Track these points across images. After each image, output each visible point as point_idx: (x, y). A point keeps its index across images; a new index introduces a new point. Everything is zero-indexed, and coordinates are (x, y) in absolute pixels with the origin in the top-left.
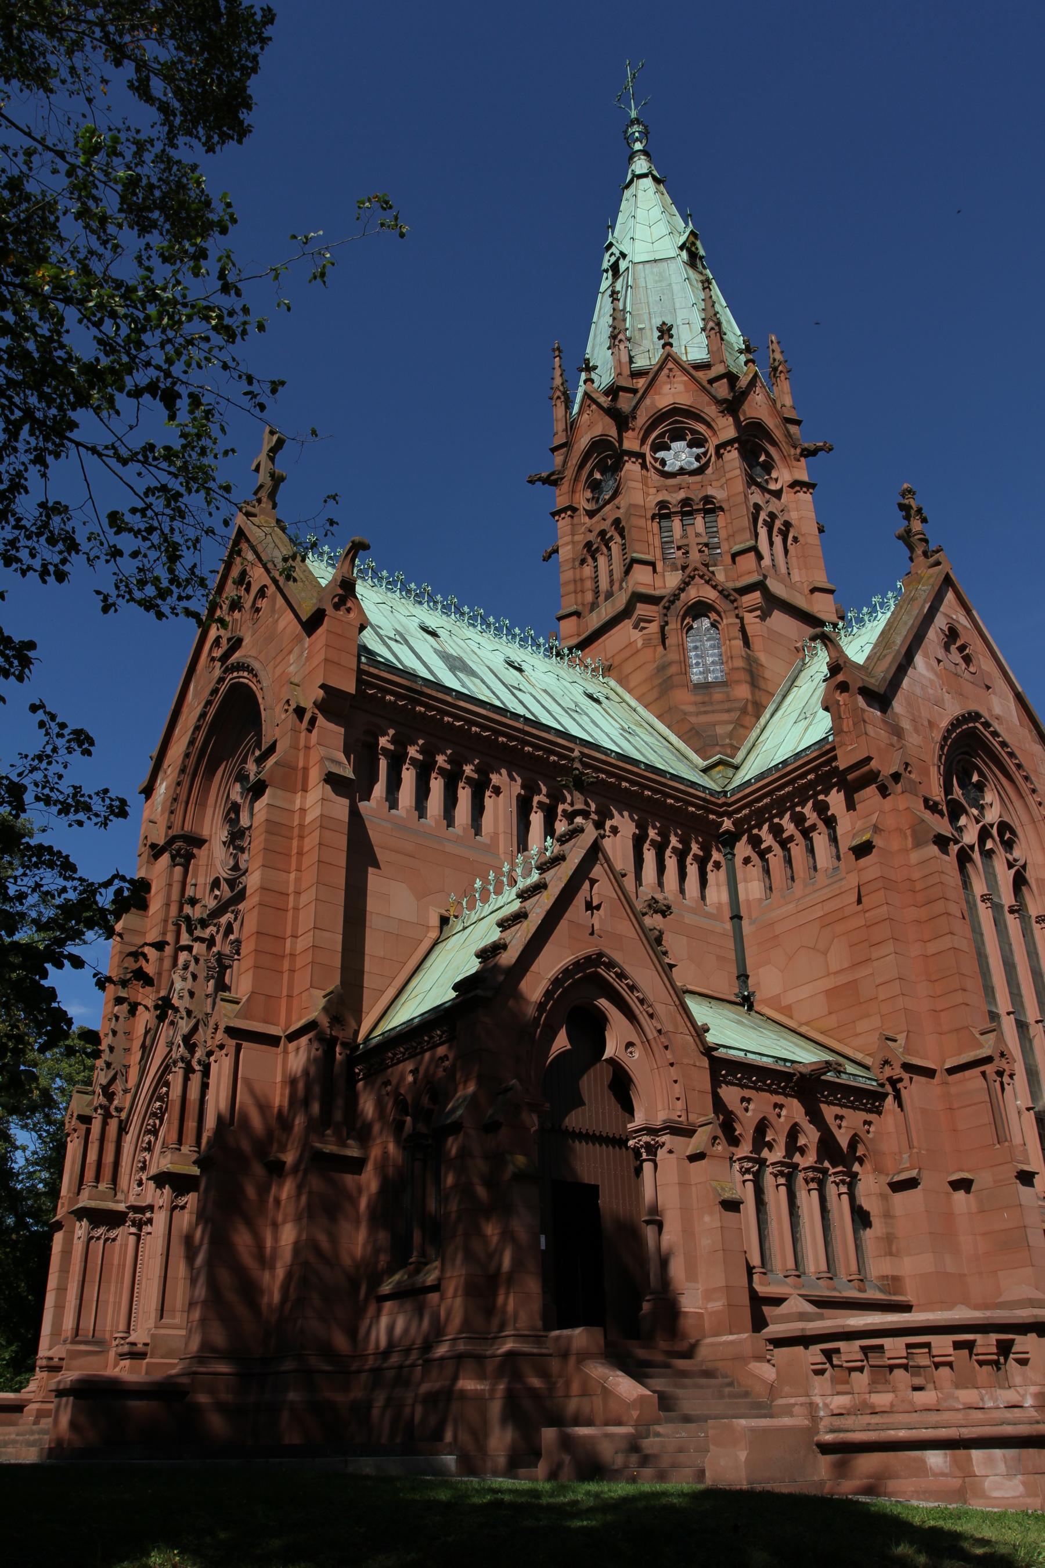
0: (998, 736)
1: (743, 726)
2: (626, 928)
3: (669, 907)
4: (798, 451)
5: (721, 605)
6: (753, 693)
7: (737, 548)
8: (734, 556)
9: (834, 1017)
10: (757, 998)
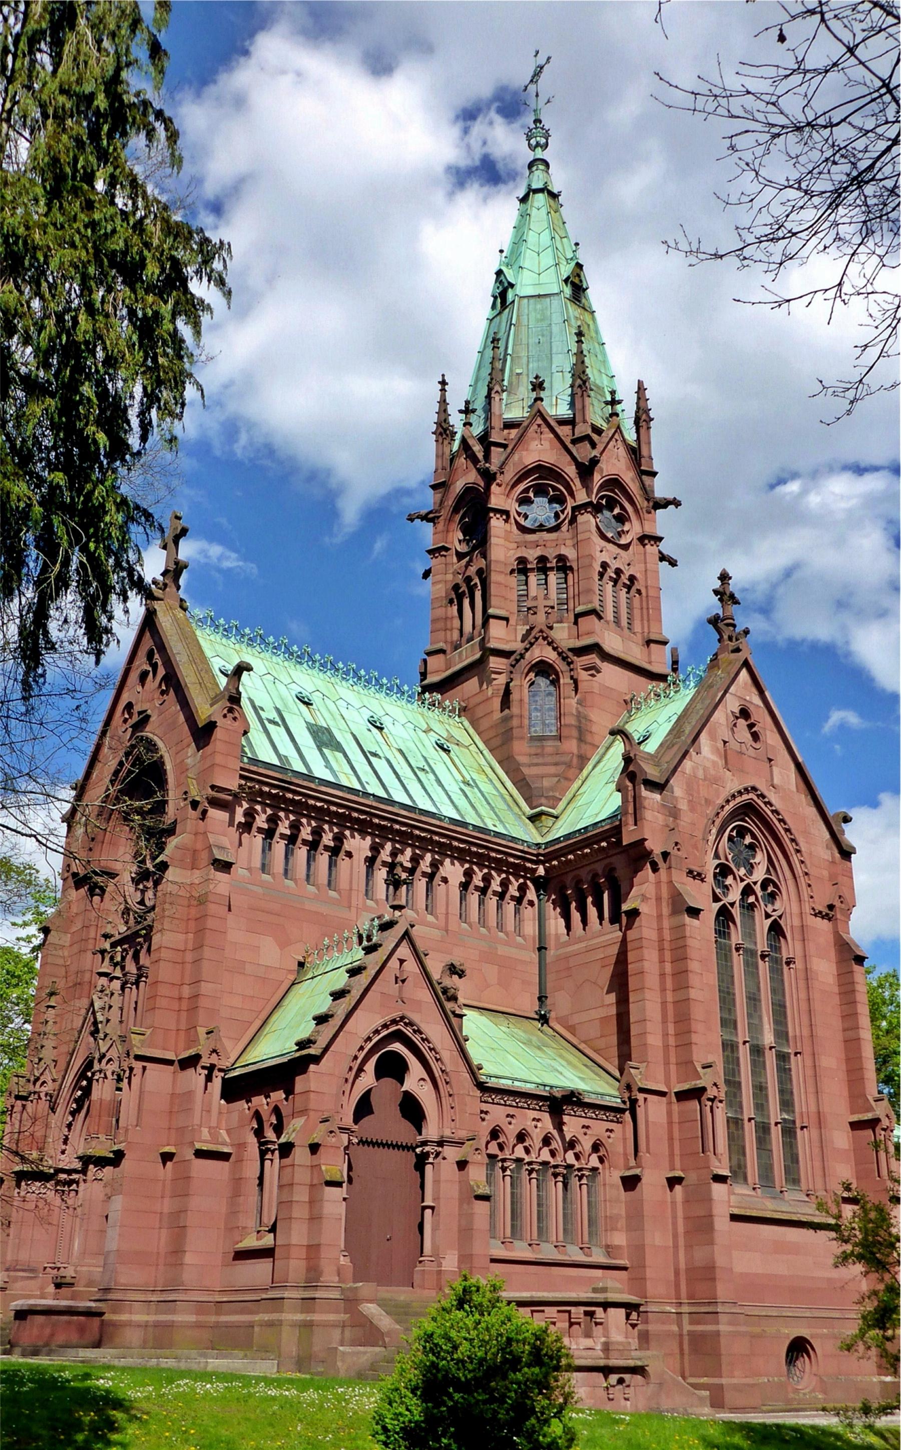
0: (771, 805)
1: (566, 779)
2: (425, 995)
3: (463, 972)
4: (651, 504)
5: (560, 666)
6: (579, 747)
7: (580, 609)
8: (578, 616)
9: (603, 1039)
10: (552, 1016)
